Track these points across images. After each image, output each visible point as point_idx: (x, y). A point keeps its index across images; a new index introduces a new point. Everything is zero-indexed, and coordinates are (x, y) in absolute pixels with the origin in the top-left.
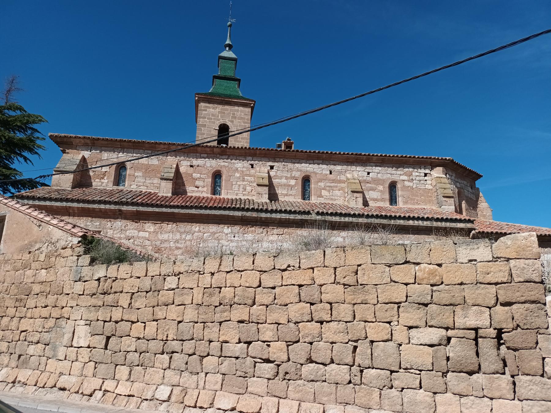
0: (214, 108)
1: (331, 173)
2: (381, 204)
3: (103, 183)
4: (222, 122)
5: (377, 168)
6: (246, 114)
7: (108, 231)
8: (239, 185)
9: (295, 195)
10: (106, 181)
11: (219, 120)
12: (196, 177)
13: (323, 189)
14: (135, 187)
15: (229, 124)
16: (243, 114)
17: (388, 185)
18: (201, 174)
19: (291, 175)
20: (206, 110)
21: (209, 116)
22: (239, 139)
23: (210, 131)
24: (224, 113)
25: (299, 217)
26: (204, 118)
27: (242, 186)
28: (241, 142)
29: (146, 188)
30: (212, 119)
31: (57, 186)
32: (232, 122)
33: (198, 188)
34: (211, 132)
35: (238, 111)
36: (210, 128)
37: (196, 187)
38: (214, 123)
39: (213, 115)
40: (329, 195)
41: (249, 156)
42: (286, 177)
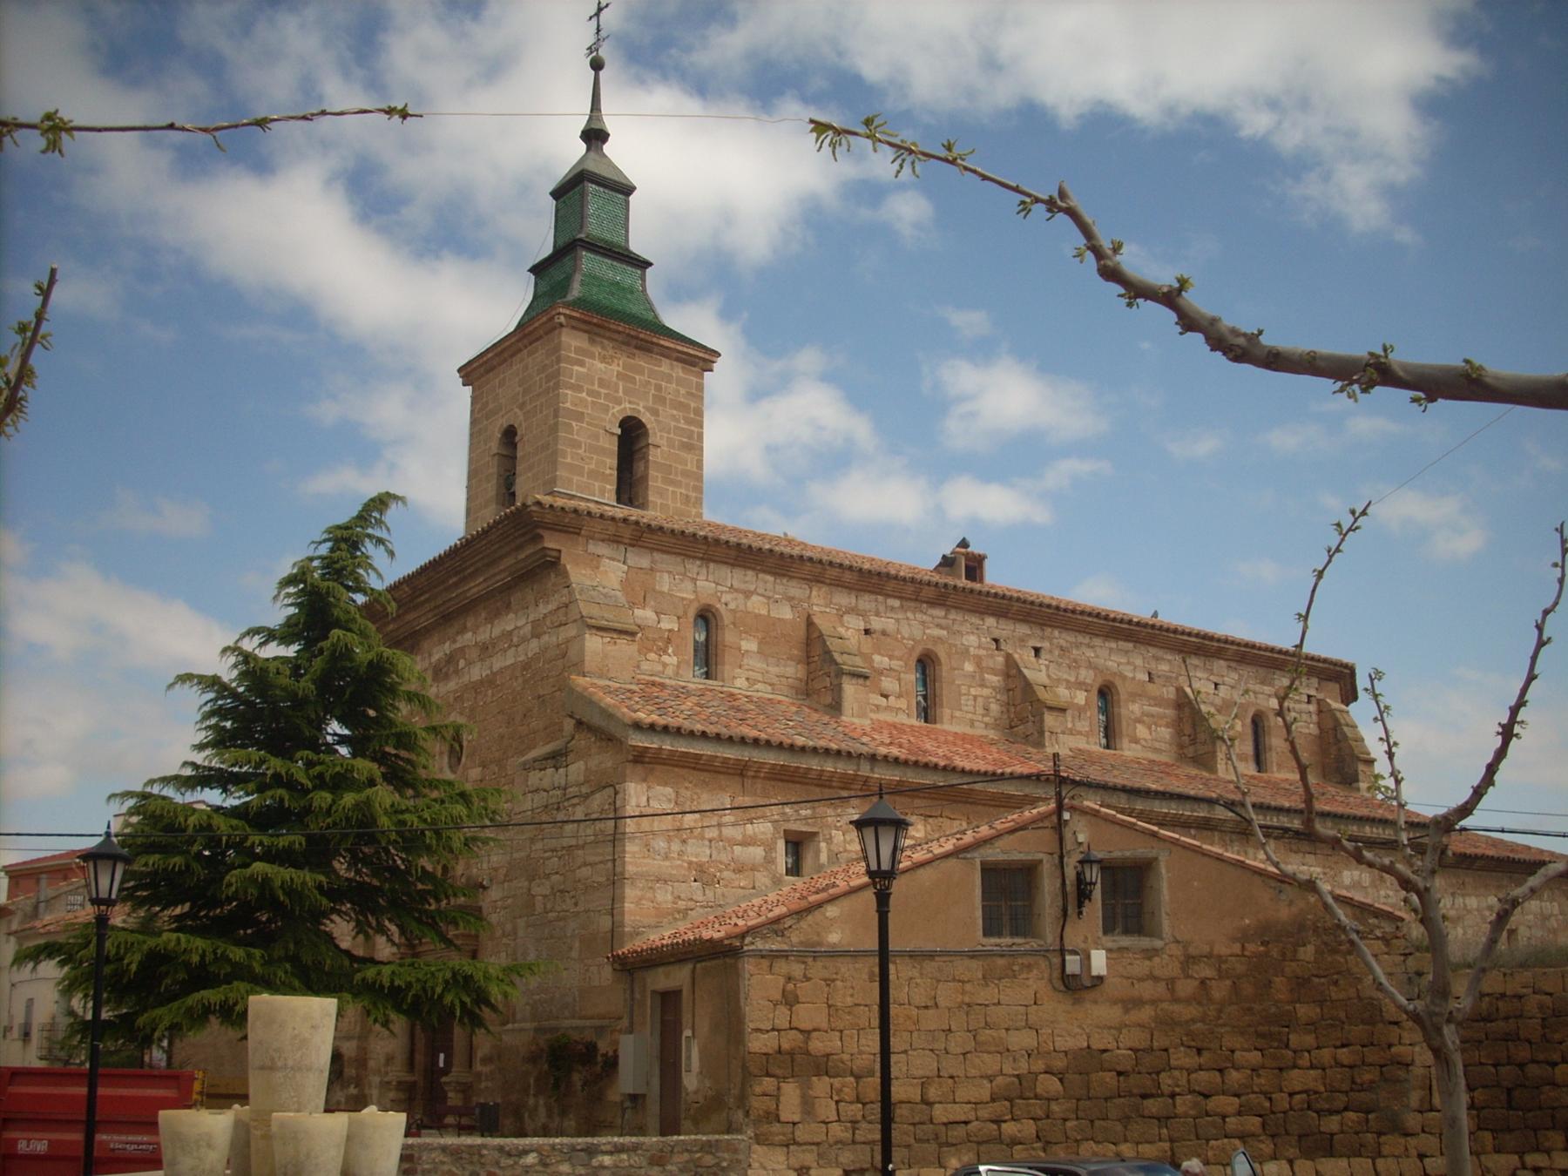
0: (603, 359)
1: (1151, 680)
2: (1081, 743)
3: (665, 665)
4: (625, 408)
5: (1064, 635)
6: (692, 394)
7: (834, 832)
8: (975, 698)
9: (1087, 735)
10: (674, 660)
11: (620, 404)
12: (882, 666)
13: (1139, 722)
14: (745, 684)
15: (646, 418)
16: (683, 391)
17: (939, 654)
18: (891, 657)
19: (1077, 678)
20: (582, 364)
21: (593, 384)
22: (676, 475)
23: (596, 437)
24: (633, 381)
25: (730, 753)
26: (579, 389)
27: (980, 700)
28: (680, 487)
29: (769, 688)
30: (597, 395)
31: (601, 677)
32: (655, 413)
33: (886, 696)
34: (598, 441)
35: (669, 379)
36: (596, 426)
37: (882, 695)
38: (606, 409)
39: (602, 383)
40: (1149, 737)
41: (993, 615)
42: (1068, 681)
